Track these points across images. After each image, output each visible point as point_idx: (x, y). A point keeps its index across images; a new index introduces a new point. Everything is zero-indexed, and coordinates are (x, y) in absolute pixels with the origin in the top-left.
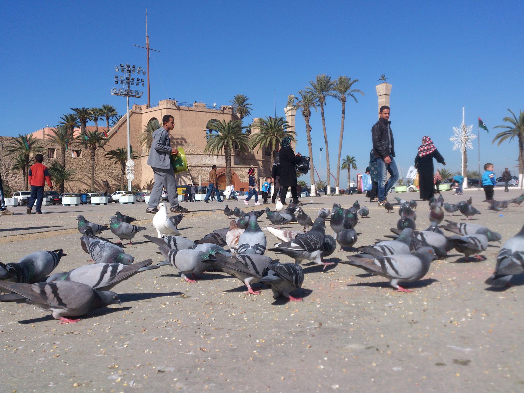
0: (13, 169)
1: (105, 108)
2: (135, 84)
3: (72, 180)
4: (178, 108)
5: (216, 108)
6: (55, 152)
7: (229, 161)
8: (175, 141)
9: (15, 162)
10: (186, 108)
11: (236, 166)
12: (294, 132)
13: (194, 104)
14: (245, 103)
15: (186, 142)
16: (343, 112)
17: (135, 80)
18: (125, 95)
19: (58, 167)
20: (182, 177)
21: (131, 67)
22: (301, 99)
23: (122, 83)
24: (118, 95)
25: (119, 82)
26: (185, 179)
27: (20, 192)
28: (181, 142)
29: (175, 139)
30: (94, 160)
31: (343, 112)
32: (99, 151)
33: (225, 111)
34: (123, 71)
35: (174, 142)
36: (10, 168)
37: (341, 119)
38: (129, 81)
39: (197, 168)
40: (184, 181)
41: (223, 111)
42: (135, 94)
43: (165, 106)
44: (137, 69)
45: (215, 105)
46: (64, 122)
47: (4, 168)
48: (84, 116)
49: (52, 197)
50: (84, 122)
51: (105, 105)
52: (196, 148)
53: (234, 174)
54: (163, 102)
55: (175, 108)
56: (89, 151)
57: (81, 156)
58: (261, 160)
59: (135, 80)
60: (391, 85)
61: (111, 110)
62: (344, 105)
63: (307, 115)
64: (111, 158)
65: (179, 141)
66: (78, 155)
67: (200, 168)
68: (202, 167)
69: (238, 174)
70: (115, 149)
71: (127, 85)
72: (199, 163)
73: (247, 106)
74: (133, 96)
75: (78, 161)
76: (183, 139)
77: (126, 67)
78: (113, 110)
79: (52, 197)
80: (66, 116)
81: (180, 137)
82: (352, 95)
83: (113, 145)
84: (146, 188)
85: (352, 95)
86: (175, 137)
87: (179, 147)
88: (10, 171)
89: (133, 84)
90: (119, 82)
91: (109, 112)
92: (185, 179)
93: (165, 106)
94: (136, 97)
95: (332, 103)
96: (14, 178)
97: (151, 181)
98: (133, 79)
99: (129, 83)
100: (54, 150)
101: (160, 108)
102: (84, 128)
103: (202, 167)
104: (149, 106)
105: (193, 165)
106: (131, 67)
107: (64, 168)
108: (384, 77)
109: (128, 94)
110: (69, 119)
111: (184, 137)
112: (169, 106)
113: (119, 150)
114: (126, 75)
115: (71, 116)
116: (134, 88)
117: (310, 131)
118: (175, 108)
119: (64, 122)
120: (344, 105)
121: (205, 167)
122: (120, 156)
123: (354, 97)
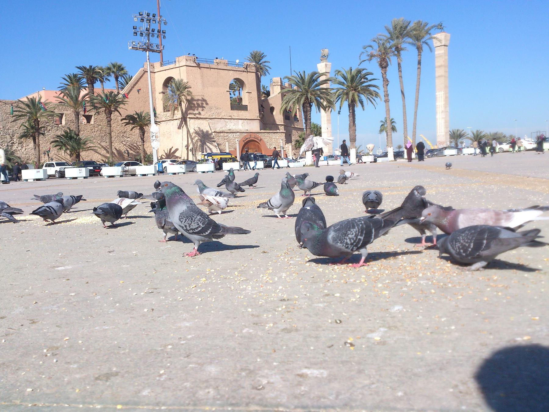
0: (21, 137)
1: (114, 66)
2: (156, 36)
3: (89, 149)
4: (198, 66)
5: (238, 65)
6: (64, 117)
7: (309, 121)
8: (195, 102)
9: (21, 131)
10: (207, 65)
11: (262, 131)
12: (375, 86)
13: (215, 61)
14: (263, 60)
15: (207, 104)
16: (419, 63)
17: (156, 32)
18: (144, 50)
19: (73, 135)
20: (208, 144)
21: (151, 16)
22: (376, 46)
23: (142, 34)
24: (137, 49)
25: (139, 33)
26: (211, 146)
27: (54, 163)
28: (202, 104)
29: (195, 100)
30: (111, 126)
31: (419, 63)
32: (115, 115)
33: (248, 68)
34: (142, 20)
35: (194, 104)
36: (15, 137)
37: (416, 71)
38: (149, 33)
39: (222, 134)
40: (210, 149)
41: (246, 68)
42: (155, 48)
43: (184, 63)
44: (157, 18)
45: (237, 61)
46: (67, 83)
47: (8, 137)
48: (92, 75)
49: (92, 168)
50: (92, 82)
51: (113, 63)
52: (220, 111)
53: (261, 140)
54: (181, 58)
55: (195, 65)
56: (103, 116)
57: (92, 122)
58: (282, 125)
59: (156, 32)
60: (449, 35)
61: (120, 68)
62: (420, 55)
63: (384, 65)
64: (127, 124)
65: (200, 102)
66: (89, 120)
67: (226, 134)
68: (227, 133)
69: (265, 140)
70: (131, 112)
71: (146, 37)
72: (223, 129)
73: (265, 64)
74: (153, 51)
75: (89, 127)
76: (204, 100)
77: (145, 15)
78: (122, 69)
79: (92, 168)
80: (69, 77)
81: (200, 98)
82: (426, 43)
83: (130, 108)
84: (164, 157)
85: (426, 43)
86: (196, 98)
87: (200, 109)
88: (15, 140)
89: (153, 36)
90: (139, 33)
91: (118, 71)
92: (211, 146)
93: (184, 63)
94: (156, 51)
95: (409, 53)
96: (20, 148)
97: (171, 149)
98: (153, 31)
99: (149, 35)
100: (62, 114)
101: (178, 66)
102: (96, 89)
103: (227, 133)
104: (162, 65)
105: (217, 130)
106: (151, 16)
107: (78, 135)
108: (441, 26)
109: (148, 48)
110: (73, 80)
111: (205, 98)
112: (189, 63)
113: (137, 114)
114: (144, 26)
115: (75, 76)
116: (155, 41)
117: (387, 85)
118: (195, 65)
119: (67, 83)
120: (420, 55)
121: (231, 133)
122: (139, 122)
123: (428, 45)
